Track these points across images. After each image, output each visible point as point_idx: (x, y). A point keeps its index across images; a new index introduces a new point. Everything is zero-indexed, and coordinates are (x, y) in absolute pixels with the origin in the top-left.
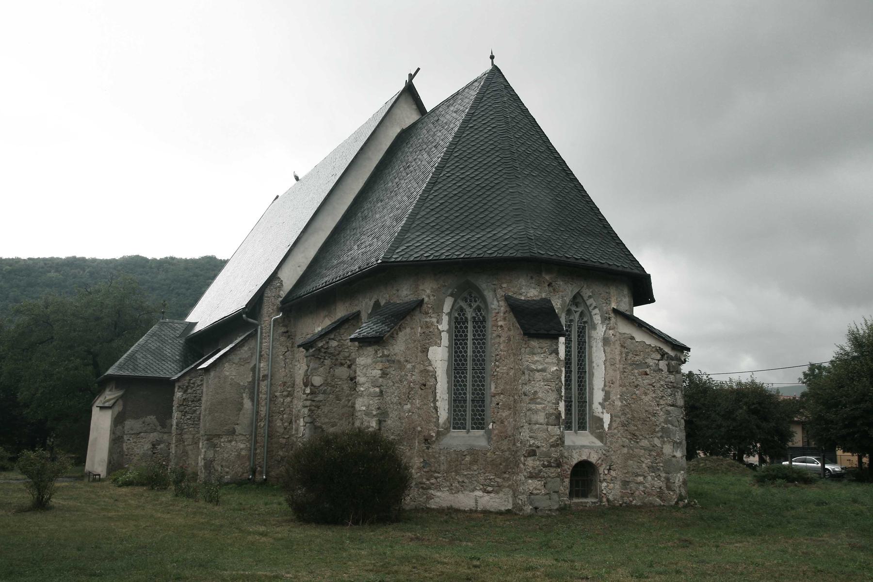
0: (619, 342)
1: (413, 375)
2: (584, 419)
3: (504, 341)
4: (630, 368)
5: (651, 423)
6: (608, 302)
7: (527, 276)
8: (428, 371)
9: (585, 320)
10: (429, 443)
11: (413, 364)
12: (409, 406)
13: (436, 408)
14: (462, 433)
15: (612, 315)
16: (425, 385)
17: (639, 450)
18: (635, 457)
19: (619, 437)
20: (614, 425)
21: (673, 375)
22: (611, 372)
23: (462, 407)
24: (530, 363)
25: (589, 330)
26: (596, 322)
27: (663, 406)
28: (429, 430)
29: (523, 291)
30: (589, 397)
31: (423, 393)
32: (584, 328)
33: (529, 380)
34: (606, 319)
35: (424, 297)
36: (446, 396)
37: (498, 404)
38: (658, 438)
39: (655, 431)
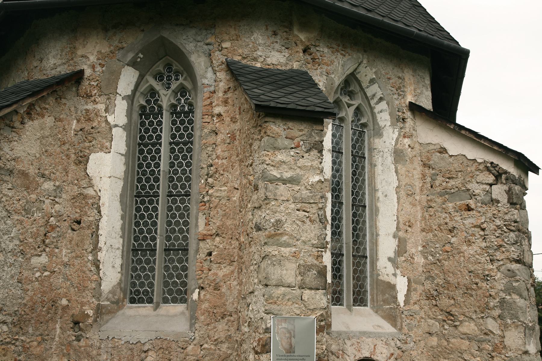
0: (419, 158)
1: (57, 203)
2: (362, 286)
3: (224, 141)
4: (439, 200)
5: (479, 292)
6: (401, 93)
7: (267, 29)
8: (85, 197)
9: (363, 121)
10: (80, 329)
11: (57, 183)
12: (44, 259)
13: (97, 264)
14: (145, 309)
15: (408, 114)
16: (79, 223)
17: (459, 340)
18: (452, 352)
19: (422, 318)
20: (415, 297)
21: (516, 209)
22: (408, 207)
23: (148, 262)
24: (267, 165)
25: (369, 139)
26: (382, 124)
27: (501, 263)
28: (83, 304)
29: (259, 53)
30: (371, 250)
31: (75, 237)
32: (362, 133)
33: (266, 198)
34: (398, 120)
35: (85, 67)
36: (118, 243)
37: (210, 254)
38: (494, 318)
39: (487, 307)
